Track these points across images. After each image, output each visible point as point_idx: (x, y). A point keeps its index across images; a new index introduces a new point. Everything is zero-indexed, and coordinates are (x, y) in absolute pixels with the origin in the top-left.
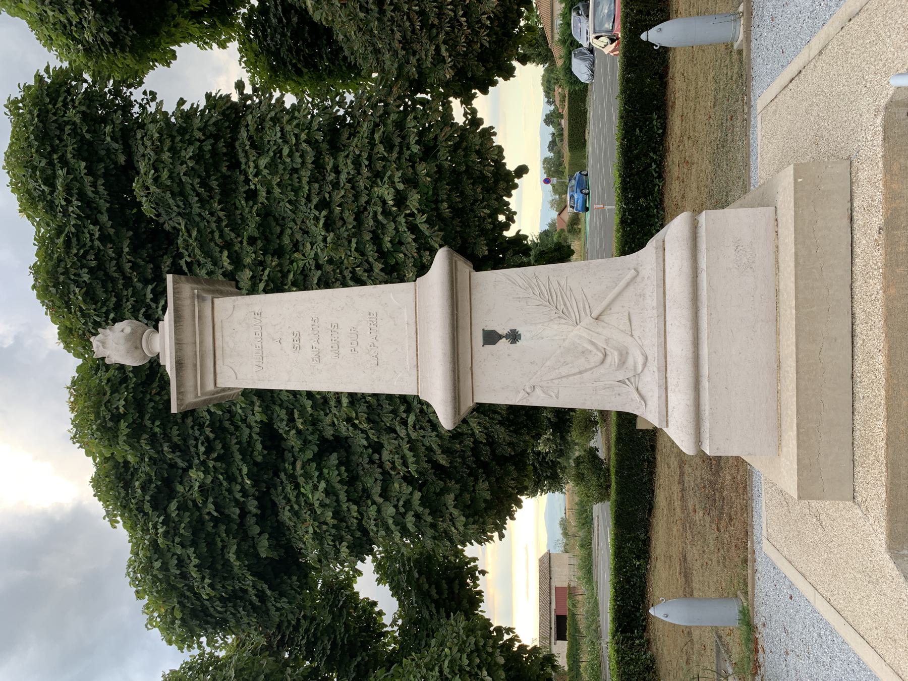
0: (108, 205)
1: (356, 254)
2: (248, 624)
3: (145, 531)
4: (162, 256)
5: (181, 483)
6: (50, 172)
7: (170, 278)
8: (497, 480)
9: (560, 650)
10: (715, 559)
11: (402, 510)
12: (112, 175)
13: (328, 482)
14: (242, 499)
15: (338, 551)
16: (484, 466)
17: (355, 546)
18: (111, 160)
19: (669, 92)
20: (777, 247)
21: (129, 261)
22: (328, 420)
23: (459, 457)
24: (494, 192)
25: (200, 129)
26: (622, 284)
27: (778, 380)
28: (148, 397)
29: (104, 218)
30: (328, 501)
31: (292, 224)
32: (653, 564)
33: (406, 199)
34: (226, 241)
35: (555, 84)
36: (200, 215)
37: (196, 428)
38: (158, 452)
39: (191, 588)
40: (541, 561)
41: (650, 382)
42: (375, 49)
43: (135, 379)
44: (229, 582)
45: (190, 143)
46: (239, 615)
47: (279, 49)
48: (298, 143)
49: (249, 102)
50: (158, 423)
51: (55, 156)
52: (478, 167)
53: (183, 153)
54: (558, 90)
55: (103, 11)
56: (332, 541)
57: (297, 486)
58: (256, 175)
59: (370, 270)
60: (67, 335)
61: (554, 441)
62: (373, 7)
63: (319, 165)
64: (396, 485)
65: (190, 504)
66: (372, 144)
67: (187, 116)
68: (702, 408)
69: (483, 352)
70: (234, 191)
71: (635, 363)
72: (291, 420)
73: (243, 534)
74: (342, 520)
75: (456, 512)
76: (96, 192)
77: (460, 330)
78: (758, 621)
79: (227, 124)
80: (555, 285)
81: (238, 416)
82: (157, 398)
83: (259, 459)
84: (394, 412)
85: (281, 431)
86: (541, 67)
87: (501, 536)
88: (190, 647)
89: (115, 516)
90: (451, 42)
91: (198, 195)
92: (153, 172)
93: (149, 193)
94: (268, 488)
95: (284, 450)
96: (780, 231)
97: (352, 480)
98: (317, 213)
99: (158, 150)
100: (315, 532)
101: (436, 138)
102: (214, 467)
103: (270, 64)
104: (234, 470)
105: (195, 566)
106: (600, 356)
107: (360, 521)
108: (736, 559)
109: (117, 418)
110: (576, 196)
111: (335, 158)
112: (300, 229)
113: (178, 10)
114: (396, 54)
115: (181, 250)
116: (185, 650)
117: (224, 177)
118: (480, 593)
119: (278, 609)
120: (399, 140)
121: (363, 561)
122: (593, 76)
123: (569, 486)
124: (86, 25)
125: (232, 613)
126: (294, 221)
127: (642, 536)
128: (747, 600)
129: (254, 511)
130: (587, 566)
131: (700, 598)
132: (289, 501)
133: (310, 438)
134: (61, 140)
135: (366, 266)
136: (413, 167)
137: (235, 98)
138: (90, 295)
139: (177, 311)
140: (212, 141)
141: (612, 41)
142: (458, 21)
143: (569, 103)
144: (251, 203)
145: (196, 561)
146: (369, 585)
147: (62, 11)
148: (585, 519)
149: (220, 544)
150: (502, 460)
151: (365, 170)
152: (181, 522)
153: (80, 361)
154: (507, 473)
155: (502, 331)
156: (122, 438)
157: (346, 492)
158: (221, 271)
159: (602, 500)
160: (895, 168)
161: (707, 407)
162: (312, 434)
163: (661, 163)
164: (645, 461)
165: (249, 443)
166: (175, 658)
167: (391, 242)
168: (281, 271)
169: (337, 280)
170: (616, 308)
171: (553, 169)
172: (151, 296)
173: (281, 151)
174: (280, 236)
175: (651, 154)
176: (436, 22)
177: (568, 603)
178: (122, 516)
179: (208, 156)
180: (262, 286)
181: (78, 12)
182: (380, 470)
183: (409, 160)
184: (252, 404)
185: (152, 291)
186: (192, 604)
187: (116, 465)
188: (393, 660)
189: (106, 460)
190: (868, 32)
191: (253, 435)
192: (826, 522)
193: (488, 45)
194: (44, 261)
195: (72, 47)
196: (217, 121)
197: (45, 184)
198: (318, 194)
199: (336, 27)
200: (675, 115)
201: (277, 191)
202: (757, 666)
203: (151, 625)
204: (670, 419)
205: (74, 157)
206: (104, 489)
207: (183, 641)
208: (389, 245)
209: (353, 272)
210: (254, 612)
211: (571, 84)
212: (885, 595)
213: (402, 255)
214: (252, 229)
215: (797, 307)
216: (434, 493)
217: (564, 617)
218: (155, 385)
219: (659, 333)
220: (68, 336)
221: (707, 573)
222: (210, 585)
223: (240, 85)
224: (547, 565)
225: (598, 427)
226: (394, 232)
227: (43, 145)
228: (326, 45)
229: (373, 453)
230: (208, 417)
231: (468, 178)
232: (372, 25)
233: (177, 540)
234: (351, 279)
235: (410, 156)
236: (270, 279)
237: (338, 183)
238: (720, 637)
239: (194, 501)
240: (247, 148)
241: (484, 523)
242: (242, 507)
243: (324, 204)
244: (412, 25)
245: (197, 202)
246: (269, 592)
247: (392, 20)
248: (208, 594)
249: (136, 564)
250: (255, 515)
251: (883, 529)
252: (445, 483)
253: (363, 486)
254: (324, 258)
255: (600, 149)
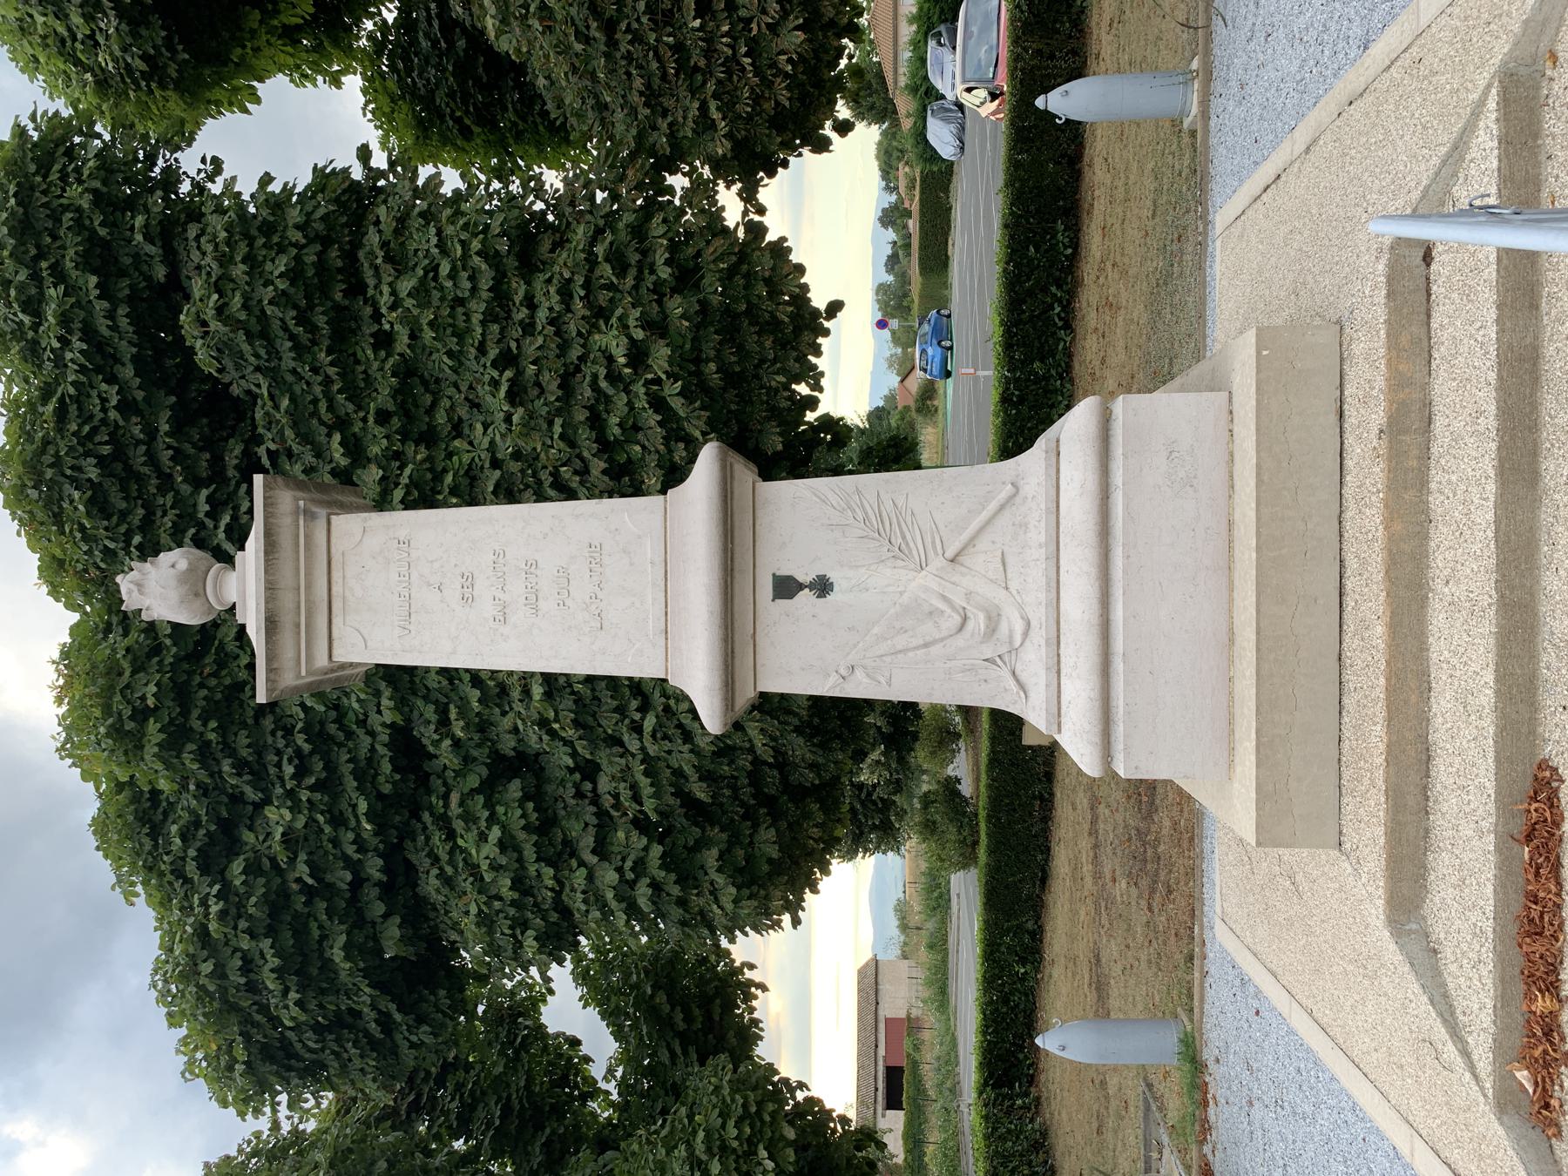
0: (134, 350)
1: (562, 445)
2: (362, 1070)
3: (186, 909)
4: (226, 440)
5: (251, 828)
6: (33, 291)
7: (258, 479)
8: (790, 826)
9: (892, 1125)
10: (1144, 958)
11: (630, 876)
12: (143, 300)
13: (504, 828)
14: (357, 856)
15: (518, 945)
16: (770, 802)
17: (548, 938)
18: (141, 273)
19: (1084, 187)
20: (1232, 454)
21: (169, 447)
22: (507, 723)
23: (728, 787)
24: (793, 348)
25: (297, 227)
26: (993, 506)
27: (1231, 661)
28: (197, 679)
29: (127, 372)
30: (503, 861)
31: (451, 391)
32: (1047, 972)
33: (647, 355)
34: (338, 417)
35: (899, 159)
36: (294, 372)
37: (280, 733)
38: (211, 775)
39: (264, 1009)
40: (862, 973)
41: (1033, 663)
42: (598, 102)
43: (174, 649)
44: (330, 998)
45: (281, 250)
46: (345, 1056)
47: (432, 92)
48: (466, 256)
49: (382, 183)
50: (213, 724)
51: (44, 265)
52: (768, 305)
53: (269, 266)
54: (903, 170)
55: (133, 19)
56: (510, 927)
57: (451, 835)
58: (393, 308)
59: (584, 472)
60: (55, 573)
61: (887, 766)
62: (597, 35)
63: (500, 293)
64: (621, 835)
65: (266, 863)
66: (592, 261)
67: (277, 204)
68: (1113, 703)
69: (774, 611)
70: (354, 332)
71: (1011, 631)
72: (444, 722)
73: (356, 918)
74: (527, 892)
75: (720, 880)
76: (114, 328)
77: (737, 574)
78: (1208, 1055)
79: (344, 219)
80: (889, 505)
81: (351, 715)
82: (213, 682)
83: (387, 789)
84: (621, 710)
85: (425, 741)
86: (875, 128)
87: (796, 922)
88: (257, 1112)
89: (133, 884)
90: (726, 98)
91: (292, 337)
92: (216, 296)
93: (207, 333)
94: (401, 839)
95: (428, 775)
96: (1236, 430)
97: (545, 826)
98: (495, 374)
99: (225, 261)
100: (480, 911)
101: (699, 254)
102: (309, 800)
103: (416, 116)
104: (344, 806)
105: (272, 971)
106: (958, 619)
107: (558, 894)
108: (1177, 956)
109: (142, 714)
110: (930, 351)
111: (528, 283)
112: (466, 399)
113: (261, 22)
114: (633, 112)
115: (261, 430)
116: (249, 1117)
117: (337, 308)
118: (755, 1022)
119: (413, 1046)
120: (637, 257)
121: (560, 962)
122: (962, 149)
123: (912, 843)
124: (101, 41)
125: (334, 1052)
126: (456, 386)
127: (1030, 925)
128: (1192, 1021)
129: (377, 875)
130: (937, 981)
131: (1118, 1020)
132: (436, 860)
133: (475, 753)
134: (55, 238)
135: (578, 464)
136: (660, 302)
137: (357, 174)
138: (98, 504)
139: (269, 534)
140: (319, 247)
141: (994, 96)
142: (738, 63)
143: (922, 192)
144: (383, 353)
145: (274, 962)
146: (567, 1009)
147: (61, 15)
148: (937, 900)
149: (316, 933)
150: (799, 794)
151: (578, 304)
152: (249, 895)
153: (75, 617)
154: (807, 816)
155: (804, 577)
156: (150, 750)
157: (535, 845)
158: (328, 468)
159: (965, 866)
160: (1404, 340)
161: (1121, 703)
162: (479, 746)
163: (1069, 303)
164: (1034, 797)
165: (369, 760)
166: (233, 1131)
167: (620, 425)
168: (431, 470)
169: (527, 486)
170: (983, 544)
171: (893, 304)
172: (207, 508)
173: (436, 268)
174: (431, 410)
175: (1053, 289)
176: (702, 63)
177: (907, 1044)
178: (145, 883)
179: (310, 272)
180: (398, 494)
181: (89, 18)
182: (593, 809)
183: (654, 291)
184: (377, 694)
185: (209, 500)
186: (265, 1036)
187: (136, 798)
188: (606, 1140)
189: (120, 787)
190: (1374, 125)
191: (378, 747)
192: (1305, 886)
193: (787, 104)
194: (18, 443)
195: (73, 76)
196: (327, 215)
197: (23, 311)
198: (499, 341)
199: (536, 63)
200: (1093, 226)
201: (429, 334)
202: (1205, 1128)
203: (192, 1073)
204: (1063, 720)
205: (76, 267)
206: (116, 837)
207: (246, 1101)
208: (617, 431)
209: (555, 474)
210: (372, 1050)
211: (926, 160)
212: (1386, 994)
213: (638, 448)
214: (383, 397)
215: (1258, 548)
216: (685, 847)
217: (900, 1070)
218: (209, 659)
219: (1048, 584)
220: (57, 573)
221: (1132, 982)
222: (299, 1003)
223: (364, 153)
224: (871, 981)
225: (961, 744)
226: (626, 409)
227: (24, 244)
228: (513, 89)
229: (583, 780)
230: (302, 715)
231: (751, 324)
232: (595, 63)
233: (243, 924)
234: (552, 486)
235: (655, 284)
236: (414, 483)
237: (532, 325)
238: (1150, 1086)
239: (273, 860)
240: (379, 261)
241: (767, 897)
242: (354, 866)
243: (507, 360)
244: (663, 68)
245: (291, 350)
246: (398, 1017)
247: (629, 57)
248: (293, 1019)
249: (169, 967)
250: (379, 884)
251: (1381, 891)
252: (704, 831)
253: (565, 835)
254: (505, 449)
255: (972, 277)
